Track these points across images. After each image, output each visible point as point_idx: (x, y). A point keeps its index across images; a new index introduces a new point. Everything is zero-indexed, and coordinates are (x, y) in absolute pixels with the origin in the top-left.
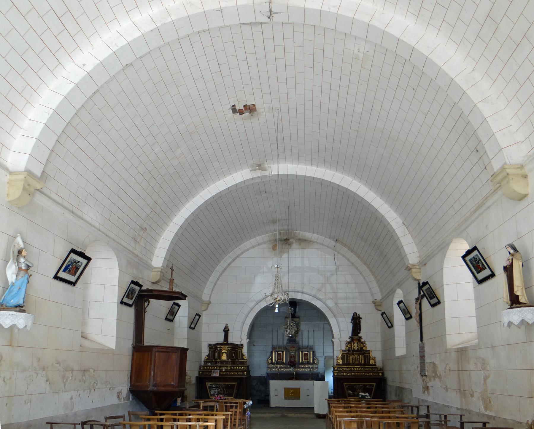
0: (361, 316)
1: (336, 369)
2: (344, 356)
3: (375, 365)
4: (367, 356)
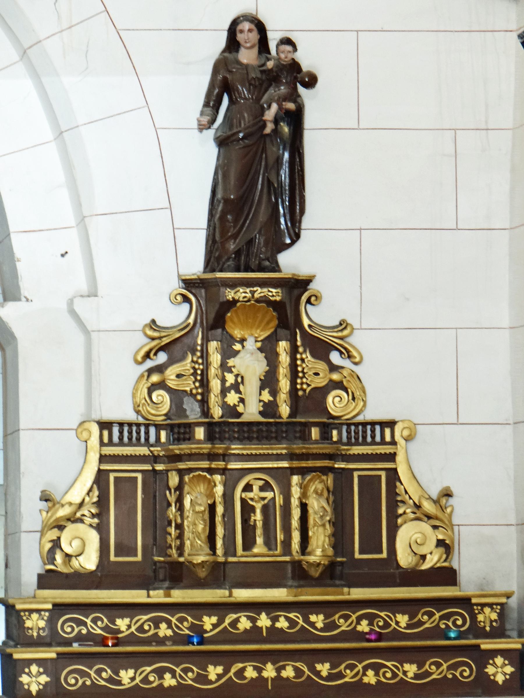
0: (306, 59)
1: (35, 624)
2: (125, 485)
3: (447, 576)
4: (369, 484)
